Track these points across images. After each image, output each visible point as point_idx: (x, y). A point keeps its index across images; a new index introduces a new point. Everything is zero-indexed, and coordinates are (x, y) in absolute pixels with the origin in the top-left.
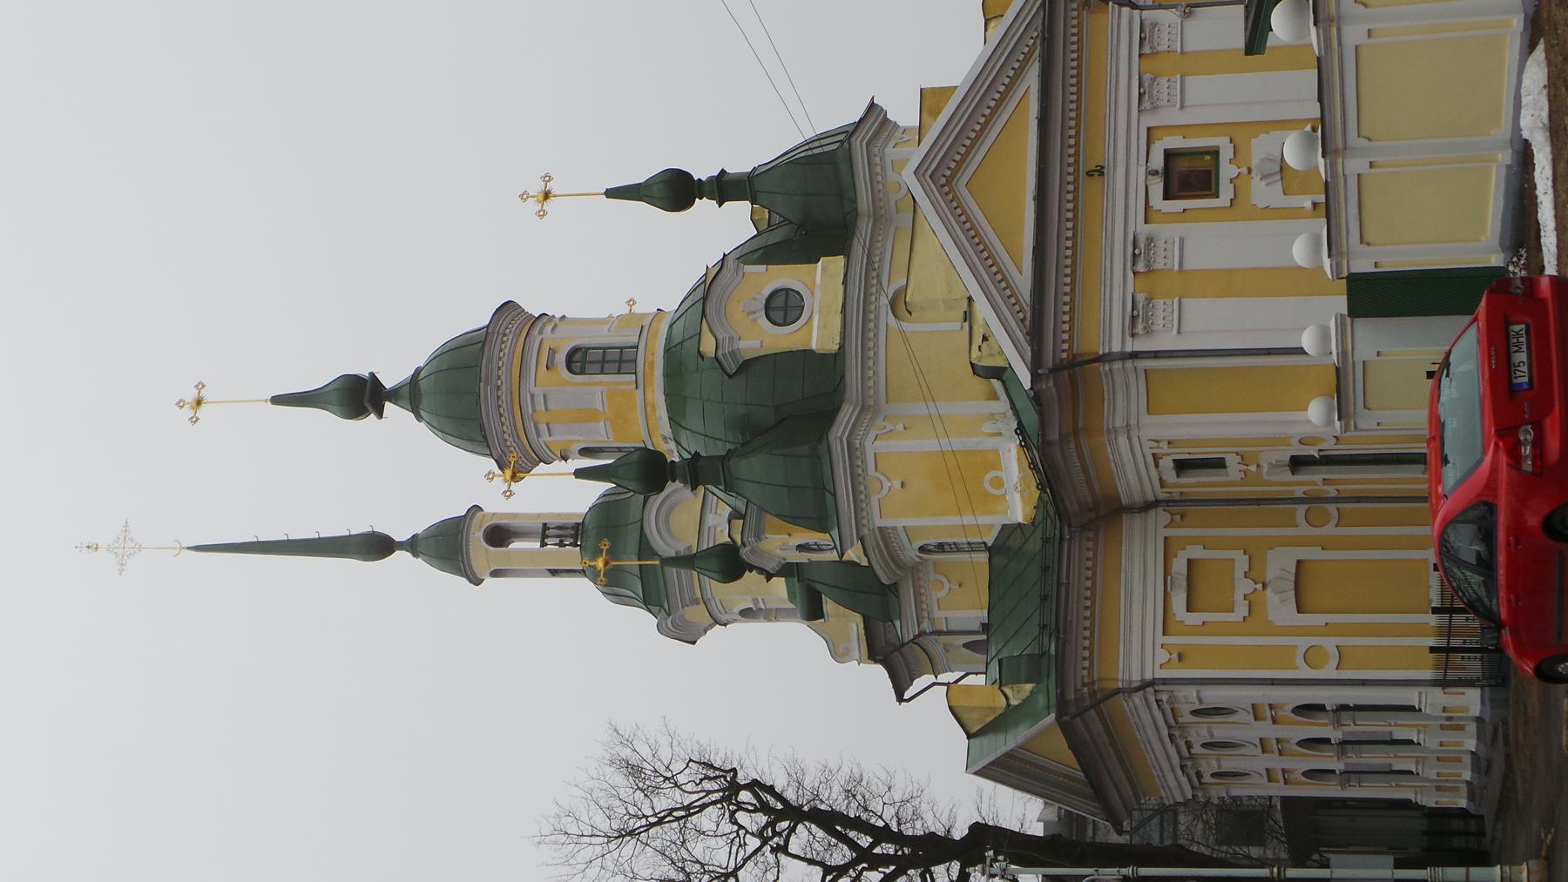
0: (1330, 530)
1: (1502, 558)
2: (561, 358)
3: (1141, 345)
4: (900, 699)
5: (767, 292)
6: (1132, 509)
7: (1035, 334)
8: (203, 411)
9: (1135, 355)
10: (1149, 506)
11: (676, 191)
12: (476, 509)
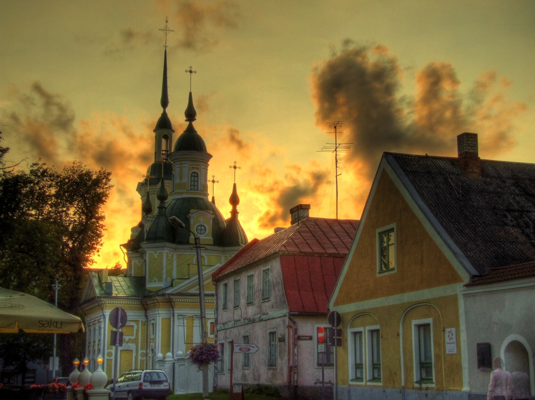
0: (140, 358)
1: (427, 294)
2: (195, 170)
3: (176, 317)
4: (121, 245)
5: (205, 225)
6: (146, 313)
7: (179, 294)
8: (188, 73)
9: (174, 316)
10: (146, 316)
11: (234, 200)
12: (174, 131)
